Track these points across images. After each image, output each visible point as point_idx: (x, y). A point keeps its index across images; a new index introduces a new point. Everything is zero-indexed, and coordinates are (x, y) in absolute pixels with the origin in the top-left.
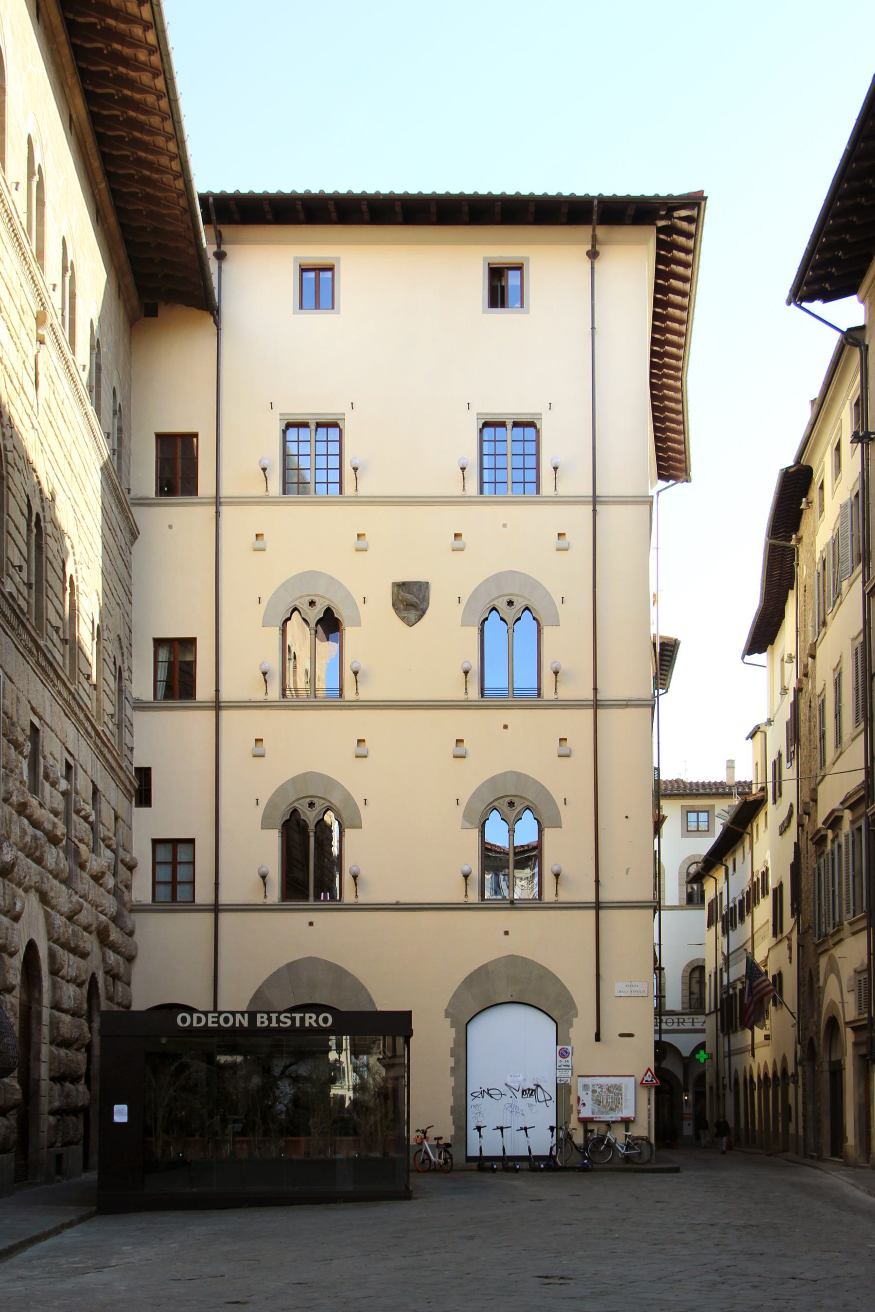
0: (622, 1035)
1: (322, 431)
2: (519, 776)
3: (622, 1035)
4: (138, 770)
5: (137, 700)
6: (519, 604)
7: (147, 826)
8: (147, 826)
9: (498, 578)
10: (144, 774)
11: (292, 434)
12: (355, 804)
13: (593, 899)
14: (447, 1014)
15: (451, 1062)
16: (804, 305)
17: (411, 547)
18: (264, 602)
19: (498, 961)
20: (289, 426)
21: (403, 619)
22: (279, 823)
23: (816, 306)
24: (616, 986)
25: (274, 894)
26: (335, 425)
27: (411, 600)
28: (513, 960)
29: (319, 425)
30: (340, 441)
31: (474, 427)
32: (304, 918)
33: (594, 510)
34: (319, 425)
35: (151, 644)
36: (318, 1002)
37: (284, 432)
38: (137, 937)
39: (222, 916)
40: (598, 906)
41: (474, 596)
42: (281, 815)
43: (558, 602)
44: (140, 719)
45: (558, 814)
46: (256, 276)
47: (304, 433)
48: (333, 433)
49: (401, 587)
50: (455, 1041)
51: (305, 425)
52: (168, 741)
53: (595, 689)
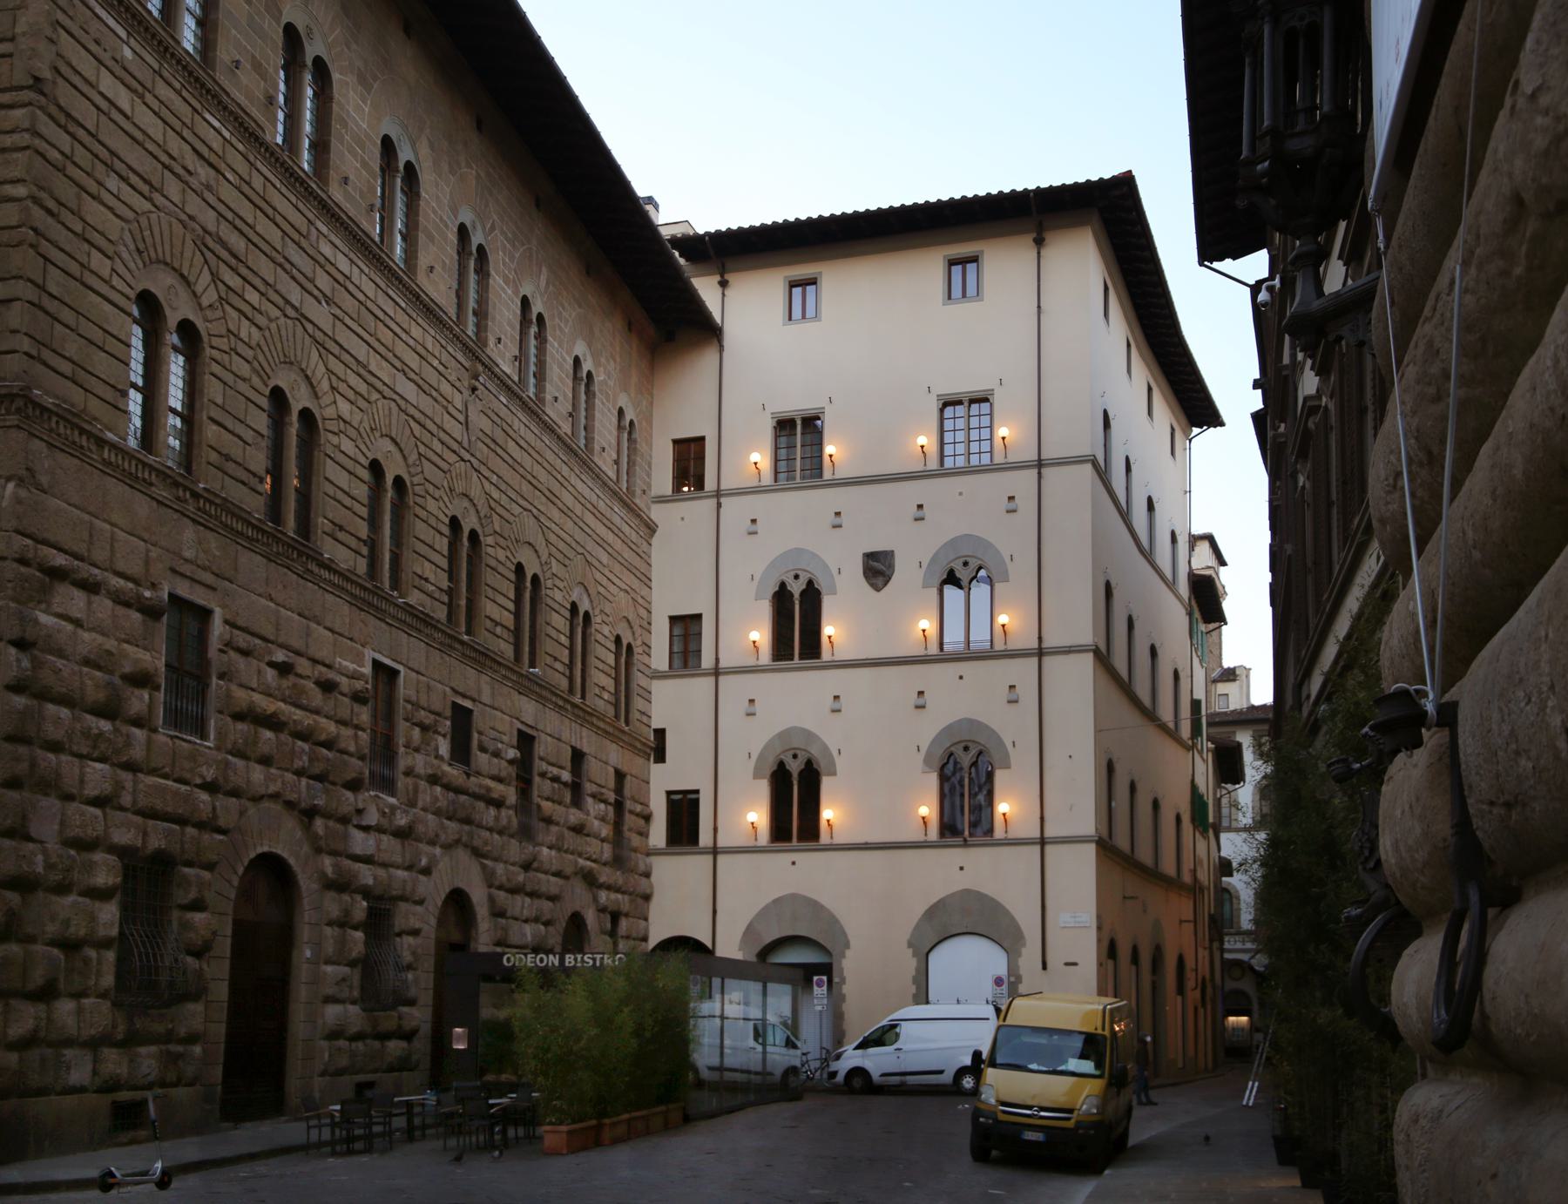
0: (1067, 964)
1: (975, 407)
2: (971, 722)
3: (1067, 964)
4: (656, 731)
5: (656, 671)
6: (973, 564)
7: (661, 781)
8: (661, 781)
9: (953, 543)
10: (660, 734)
11: (949, 411)
12: (831, 755)
13: (1038, 835)
14: (910, 945)
15: (913, 989)
16: (1216, 265)
17: (878, 521)
18: (757, 578)
19: (953, 895)
20: (946, 405)
21: (872, 585)
22: (768, 773)
23: (1227, 265)
24: (1060, 918)
25: (933, 834)
26: (986, 400)
27: (878, 568)
28: (967, 893)
29: (972, 401)
30: (991, 414)
31: (934, 407)
32: (786, 858)
33: (1039, 473)
34: (972, 401)
35: (667, 621)
36: (778, 936)
37: (942, 411)
38: (654, 878)
39: (1048, 848)
40: (1043, 842)
41: (933, 560)
42: (770, 767)
43: (1007, 560)
44: (658, 687)
45: (834, 765)
46: (746, 307)
47: (960, 410)
48: (985, 407)
49: (870, 557)
50: (917, 970)
51: (960, 403)
52: (672, 703)
53: (1040, 638)
